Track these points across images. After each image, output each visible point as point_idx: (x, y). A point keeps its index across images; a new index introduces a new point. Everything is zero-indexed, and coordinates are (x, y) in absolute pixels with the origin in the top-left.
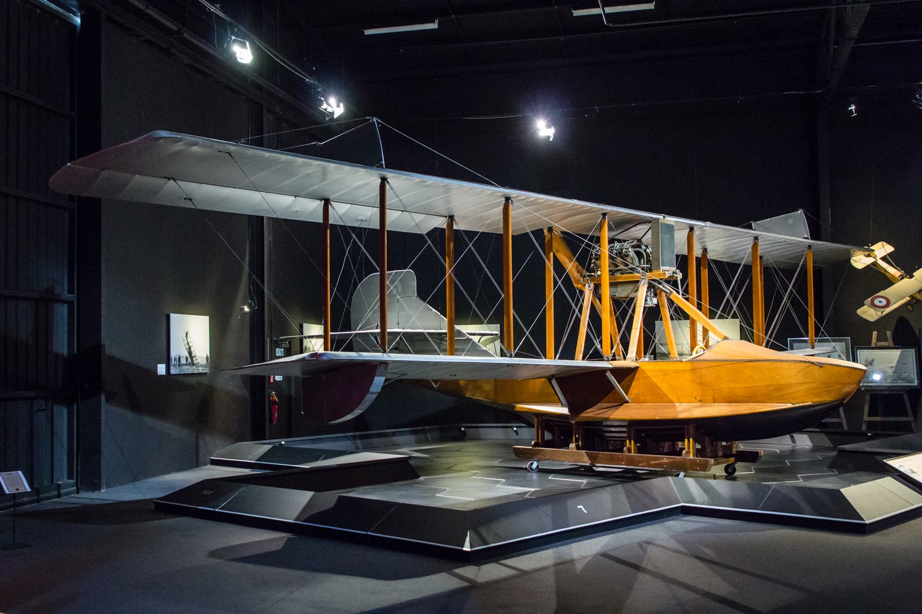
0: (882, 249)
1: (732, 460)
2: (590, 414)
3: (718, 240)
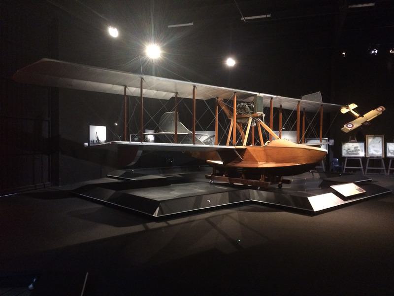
0: (353, 106)
1: (280, 183)
2: (230, 164)
3: (287, 102)
